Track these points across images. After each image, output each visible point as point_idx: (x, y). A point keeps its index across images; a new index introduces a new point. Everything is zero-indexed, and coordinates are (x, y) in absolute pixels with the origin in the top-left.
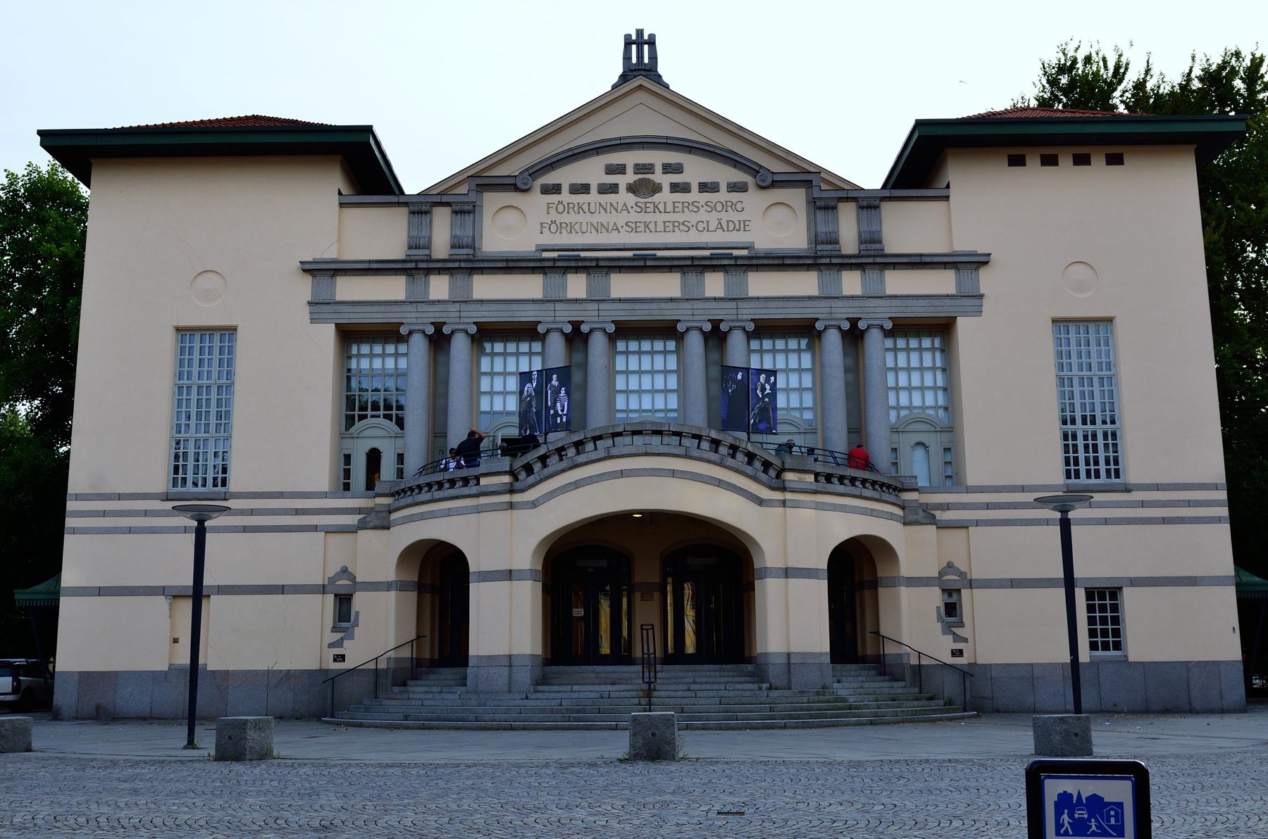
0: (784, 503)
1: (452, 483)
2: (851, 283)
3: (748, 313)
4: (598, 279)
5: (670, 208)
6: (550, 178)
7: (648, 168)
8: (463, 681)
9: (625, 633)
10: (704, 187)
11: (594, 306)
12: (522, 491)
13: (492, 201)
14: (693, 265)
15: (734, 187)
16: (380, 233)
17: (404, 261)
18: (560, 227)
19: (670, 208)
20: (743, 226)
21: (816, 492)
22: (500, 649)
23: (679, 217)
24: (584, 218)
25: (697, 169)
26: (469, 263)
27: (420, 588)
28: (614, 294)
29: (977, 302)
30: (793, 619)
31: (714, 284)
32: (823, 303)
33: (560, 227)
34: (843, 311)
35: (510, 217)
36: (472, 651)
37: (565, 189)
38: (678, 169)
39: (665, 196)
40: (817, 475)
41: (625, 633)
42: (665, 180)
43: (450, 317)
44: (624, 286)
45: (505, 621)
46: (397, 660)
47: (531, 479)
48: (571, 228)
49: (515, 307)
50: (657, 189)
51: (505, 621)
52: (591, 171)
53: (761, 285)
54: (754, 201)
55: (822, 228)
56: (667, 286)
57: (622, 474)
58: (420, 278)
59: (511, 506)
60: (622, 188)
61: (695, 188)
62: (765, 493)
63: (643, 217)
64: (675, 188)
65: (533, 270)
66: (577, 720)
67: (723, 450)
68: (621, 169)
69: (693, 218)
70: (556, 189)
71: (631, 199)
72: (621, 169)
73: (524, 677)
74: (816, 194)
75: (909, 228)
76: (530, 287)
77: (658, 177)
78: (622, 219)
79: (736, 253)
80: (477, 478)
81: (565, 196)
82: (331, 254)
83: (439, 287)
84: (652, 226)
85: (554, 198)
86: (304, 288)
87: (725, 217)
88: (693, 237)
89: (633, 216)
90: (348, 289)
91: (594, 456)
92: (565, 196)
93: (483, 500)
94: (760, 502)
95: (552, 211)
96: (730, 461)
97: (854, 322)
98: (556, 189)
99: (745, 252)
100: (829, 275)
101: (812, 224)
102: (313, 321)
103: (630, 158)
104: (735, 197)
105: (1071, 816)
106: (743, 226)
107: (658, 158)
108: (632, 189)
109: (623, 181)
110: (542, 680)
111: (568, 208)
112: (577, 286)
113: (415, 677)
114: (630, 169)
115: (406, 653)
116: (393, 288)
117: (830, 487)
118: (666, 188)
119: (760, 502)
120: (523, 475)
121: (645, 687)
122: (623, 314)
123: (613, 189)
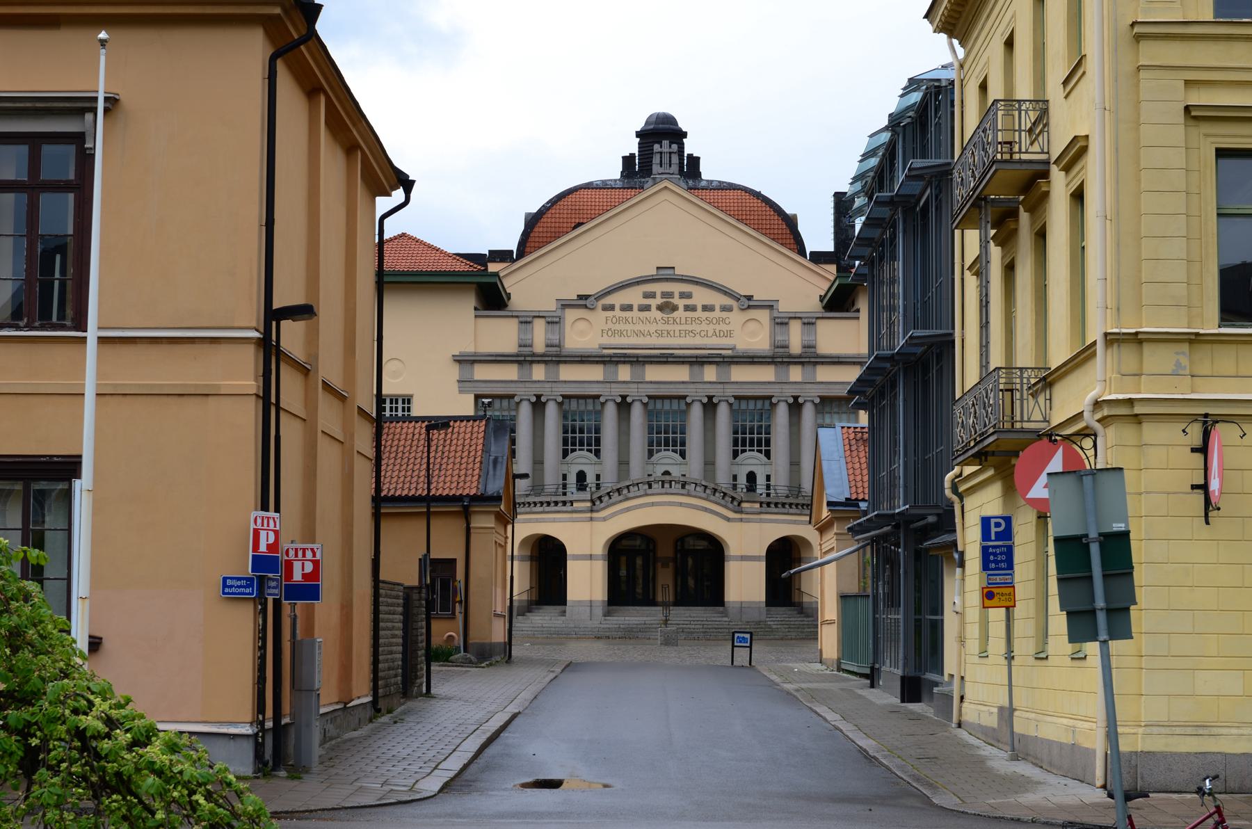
0: (741, 520)
1: (556, 503)
2: (796, 374)
3: (731, 391)
4: (638, 368)
5: (683, 321)
6: (608, 300)
7: (670, 295)
9: (274, 337)
10: (706, 308)
11: (635, 386)
12: (597, 511)
13: (571, 315)
14: (698, 362)
15: (726, 309)
16: (500, 335)
17: (517, 356)
18: (614, 333)
21: (761, 513)
22: (586, 597)
23: (689, 328)
24: (629, 327)
25: (701, 296)
27: (532, 558)
28: (648, 379)
30: (745, 583)
31: (710, 373)
32: (777, 386)
33: (614, 333)
34: (789, 391)
35: (581, 325)
36: (569, 598)
37: (617, 308)
38: (689, 296)
40: (761, 503)
41: (274, 337)
42: (681, 303)
43: (546, 391)
44: (654, 373)
45: (586, 581)
47: (602, 505)
48: (621, 333)
49: (586, 385)
50: (675, 308)
51: (586, 581)
52: (634, 296)
53: (740, 374)
54: (737, 317)
55: (779, 338)
56: (680, 374)
57: (653, 504)
58: (526, 366)
59: (591, 519)
60: (654, 308)
61: (699, 308)
62: (731, 515)
64: (687, 308)
65: (597, 362)
66: (630, 635)
67: (708, 491)
68: (651, 295)
69: (697, 328)
70: (611, 308)
71: (659, 315)
72: (651, 295)
73: (599, 612)
76: (595, 373)
77: (676, 300)
78: (653, 328)
79: (723, 352)
80: (572, 503)
81: (617, 312)
82: (470, 349)
83: (539, 372)
86: (454, 372)
87: (718, 328)
88: (698, 341)
89: (661, 327)
90: (482, 373)
91: (638, 494)
92: (617, 312)
93: (575, 515)
94: (728, 520)
96: (712, 498)
97: (796, 398)
98: (611, 308)
99: (729, 352)
100: (782, 369)
101: (773, 335)
102: (460, 392)
103: (658, 288)
104: (725, 315)
106: (729, 334)
107: (676, 288)
109: (653, 303)
110: (607, 614)
111: (619, 320)
112: (624, 373)
113: (530, 611)
114: (658, 295)
116: (510, 373)
117: (769, 510)
118: (681, 308)
119: (728, 520)
120: (598, 503)
122: (653, 391)
123: (647, 308)
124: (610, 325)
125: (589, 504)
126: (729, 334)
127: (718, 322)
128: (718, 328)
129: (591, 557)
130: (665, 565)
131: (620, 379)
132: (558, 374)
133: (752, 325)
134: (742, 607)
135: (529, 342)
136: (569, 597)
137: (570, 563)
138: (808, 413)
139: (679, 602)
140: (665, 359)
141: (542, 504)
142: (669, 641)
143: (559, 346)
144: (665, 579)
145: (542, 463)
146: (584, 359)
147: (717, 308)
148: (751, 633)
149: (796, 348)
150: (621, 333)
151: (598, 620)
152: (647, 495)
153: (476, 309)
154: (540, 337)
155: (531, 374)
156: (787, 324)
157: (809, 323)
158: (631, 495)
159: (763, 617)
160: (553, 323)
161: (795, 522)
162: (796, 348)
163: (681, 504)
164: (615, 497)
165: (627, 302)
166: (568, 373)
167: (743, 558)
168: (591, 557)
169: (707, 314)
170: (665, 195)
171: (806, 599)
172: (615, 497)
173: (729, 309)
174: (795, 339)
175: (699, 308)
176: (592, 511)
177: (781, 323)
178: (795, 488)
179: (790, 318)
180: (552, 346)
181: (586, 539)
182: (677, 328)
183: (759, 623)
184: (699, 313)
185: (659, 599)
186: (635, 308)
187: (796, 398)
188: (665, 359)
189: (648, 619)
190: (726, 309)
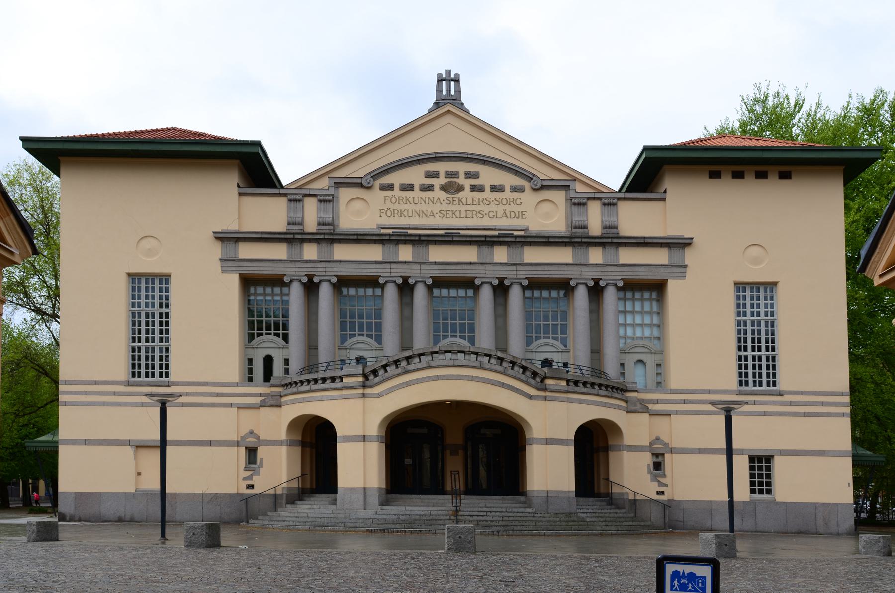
0: (545, 398)
2: (596, 255)
3: (524, 273)
5: (470, 201)
6: (386, 179)
7: (455, 174)
8: (334, 502)
10: (494, 188)
11: (418, 266)
12: (371, 386)
13: (345, 194)
15: (515, 189)
16: (268, 213)
19: (470, 201)
20: (521, 215)
21: (568, 392)
23: (477, 208)
25: (489, 176)
26: (329, 236)
27: (303, 444)
28: (432, 259)
29: (682, 270)
30: (550, 469)
31: (501, 254)
35: (358, 205)
36: (339, 485)
37: (397, 187)
38: (476, 176)
39: (467, 193)
40: (568, 381)
42: (467, 183)
43: (319, 271)
46: (289, 488)
47: (377, 379)
48: (401, 214)
49: (363, 265)
50: (460, 188)
51: (360, 466)
52: (415, 175)
53: (532, 255)
54: (529, 198)
56: (469, 254)
57: (438, 378)
58: (297, 246)
60: (437, 188)
61: (488, 188)
63: (452, 208)
64: (474, 188)
68: (436, 175)
69: (486, 209)
70: (390, 187)
71: (443, 195)
72: (436, 175)
73: (374, 500)
74: (572, 194)
75: (636, 218)
77: (462, 180)
78: (436, 208)
79: (515, 233)
80: (341, 378)
81: (397, 192)
82: (234, 227)
84: (457, 214)
85: (389, 193)
86: (217, 251)
87: (508, 209)
88: (486, 222)
89: (445, 207)
90: (246, 251)
91: (419, 366)
93: (344, 392)
94: (530, 397)
95: (388, 202)
98: (390, 187)
99: (522, 233)
101: (569, 216)
102: (223, 271)
103: (442, 167)
104: (516, 195)
105: (679, 581)
107: (462, 167)
108: (443, 188)
109: (437, 182)
110: (384, 503)
111: (399, 200)
112: (405, 253)
113: (301, 499)
114: (442, 175)
115: (295, 484)
118: (467, 188)
119: (530, 397)
120: (371, 377)
121: (454, 509)
122: (438, 272)
123: (430, 188)
124: (389, 205)
125: (361, 379)
126: (521, 215)
127: (508, 203)
128: (508, 209)
129: (364, 438)
130: (454, 453)
131: (401, 259)
132: (332, 253)
133: (546, 207)
134: (549, 497)
135: (299, 220)
136: (341, 483)
137: (340, 446)
138: (610, 296)
139: (469, 492)
140: (451, 239)
141: (308, 381)
142: (462, 545)
143: (332, 224)
144: (454, 465)
145: (316, 348)
146: (359, 238)
147: (507, 189)
148: (714, 564)
149: (595, 228)
150: (401, 214)
151: (374, 511)
152: (430, 367)
153: (239, 186)
154: (311, 216)
155: (301, 253)
156: (584, 204)
157: (609, 204)
158: (411, 367)
159: (574, 509)
160: (325, 201)
161: (605, 405)
162: (595, 228)
163: (472, 378)
164: (391, 369)
165: (407, 181)
166: (341, 252)
167: (548, 441)
168: (364, 438)
169: (496, 194)
170: (449, 119)
171: (615, 489)
172: (391, 369)
173: (521, 190)
174: (595, 220)
175: (488, 188)
176: (364, 386)
177: (578, 203)
178: (598, 371)
179: (589, 199)
180: (324, 224)
181: (359, 419)
182: (463, 208)
183: (569, 515)
184: (487, 193)
185: (448, 487)
186: (417, 188)
187: (596, 281)
188: (451, 239)
189: (434, 510)
190: (515, 189)
